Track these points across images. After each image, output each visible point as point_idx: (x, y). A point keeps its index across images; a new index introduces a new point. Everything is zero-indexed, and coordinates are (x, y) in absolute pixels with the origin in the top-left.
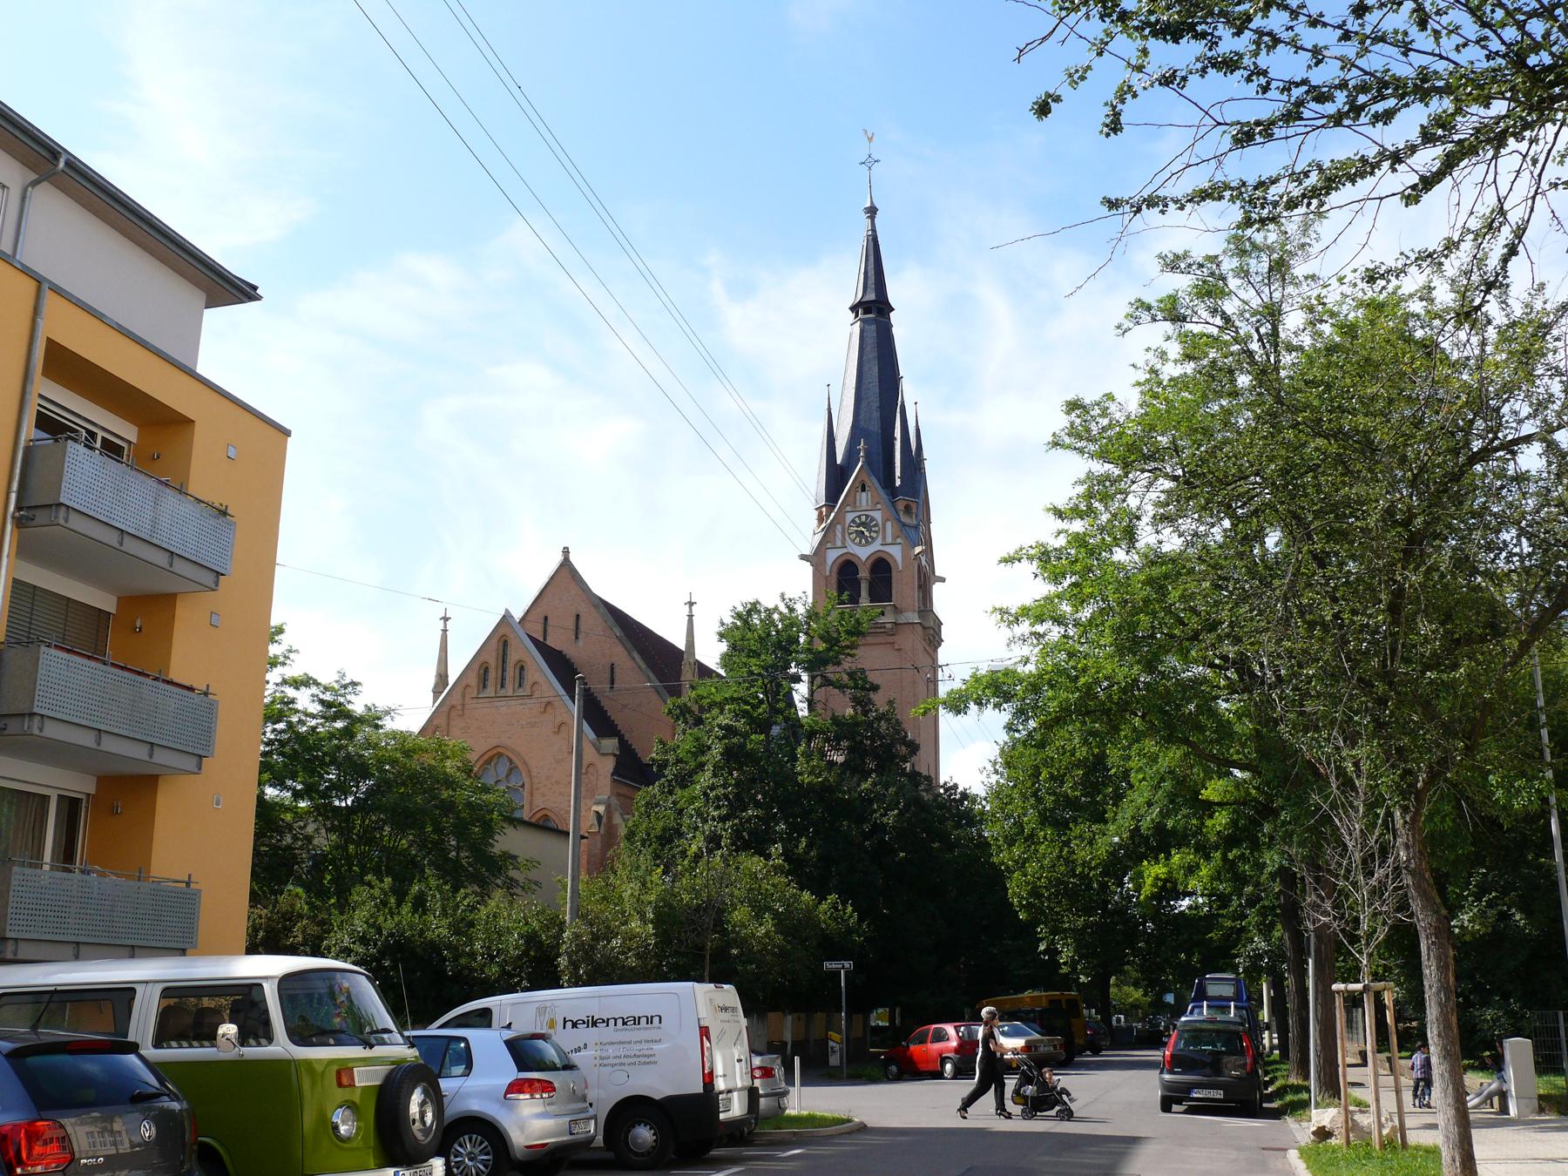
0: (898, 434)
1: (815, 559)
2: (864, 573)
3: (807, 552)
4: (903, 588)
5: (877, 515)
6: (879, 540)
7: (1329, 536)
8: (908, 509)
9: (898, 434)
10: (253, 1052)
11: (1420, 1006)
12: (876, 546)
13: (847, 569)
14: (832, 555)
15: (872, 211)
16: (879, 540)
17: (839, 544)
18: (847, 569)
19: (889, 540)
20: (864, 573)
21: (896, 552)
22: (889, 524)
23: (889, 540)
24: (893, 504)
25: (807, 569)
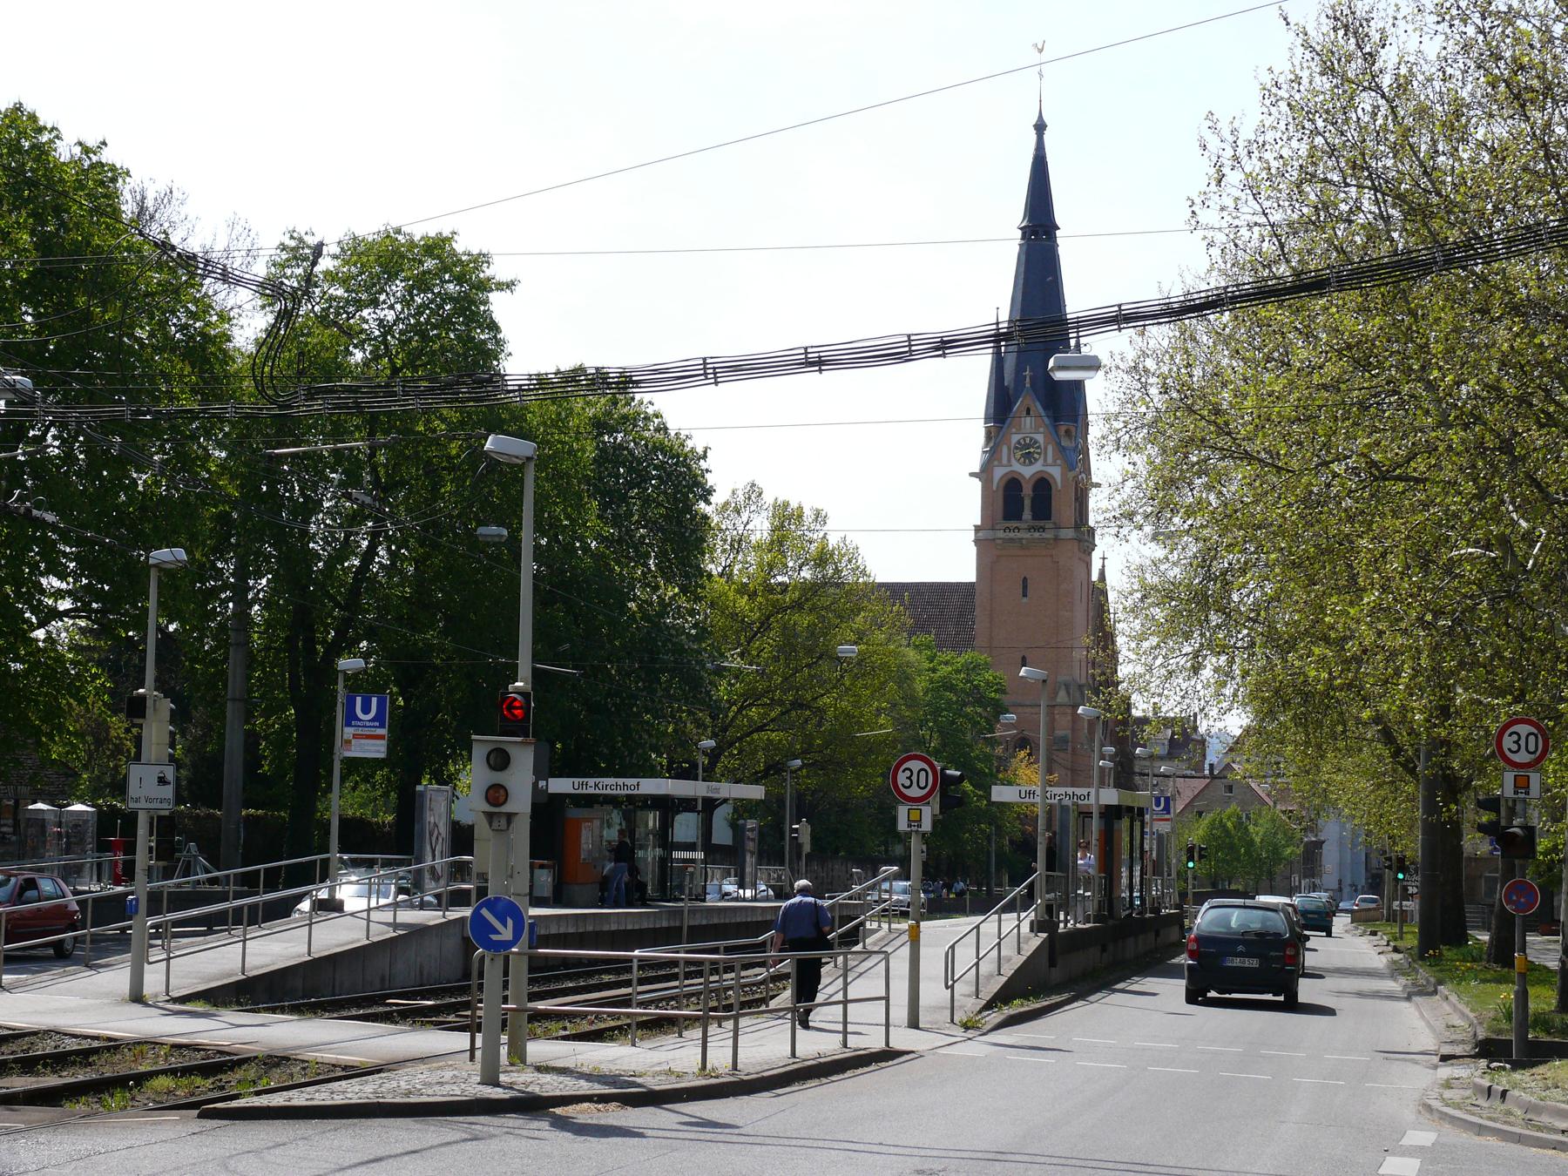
0: (606, 978)
1: (984, 474)
2: (1027, 491)
3: (977, 470)
4: (1062, 508)
5: (1040, 438)
6: (1041, 461)
7: (1392, 511)
8: (1068, 432)
9: (606, 978)
10: (1417, 917)
11: (224, 913)
12: (1038, 467)
13: (1012, 486)
14: (999, 473)
15: (1040, 127)
16: (1041, 461)
17: (1005, 461)
18: (1012, 486)
19: (1050, 460)
20: (1027, 491)
21: (1056, 472)
22: (1050, 449)
23: (1050, 460)
24: (1056, 428)
25: (977, 485)
